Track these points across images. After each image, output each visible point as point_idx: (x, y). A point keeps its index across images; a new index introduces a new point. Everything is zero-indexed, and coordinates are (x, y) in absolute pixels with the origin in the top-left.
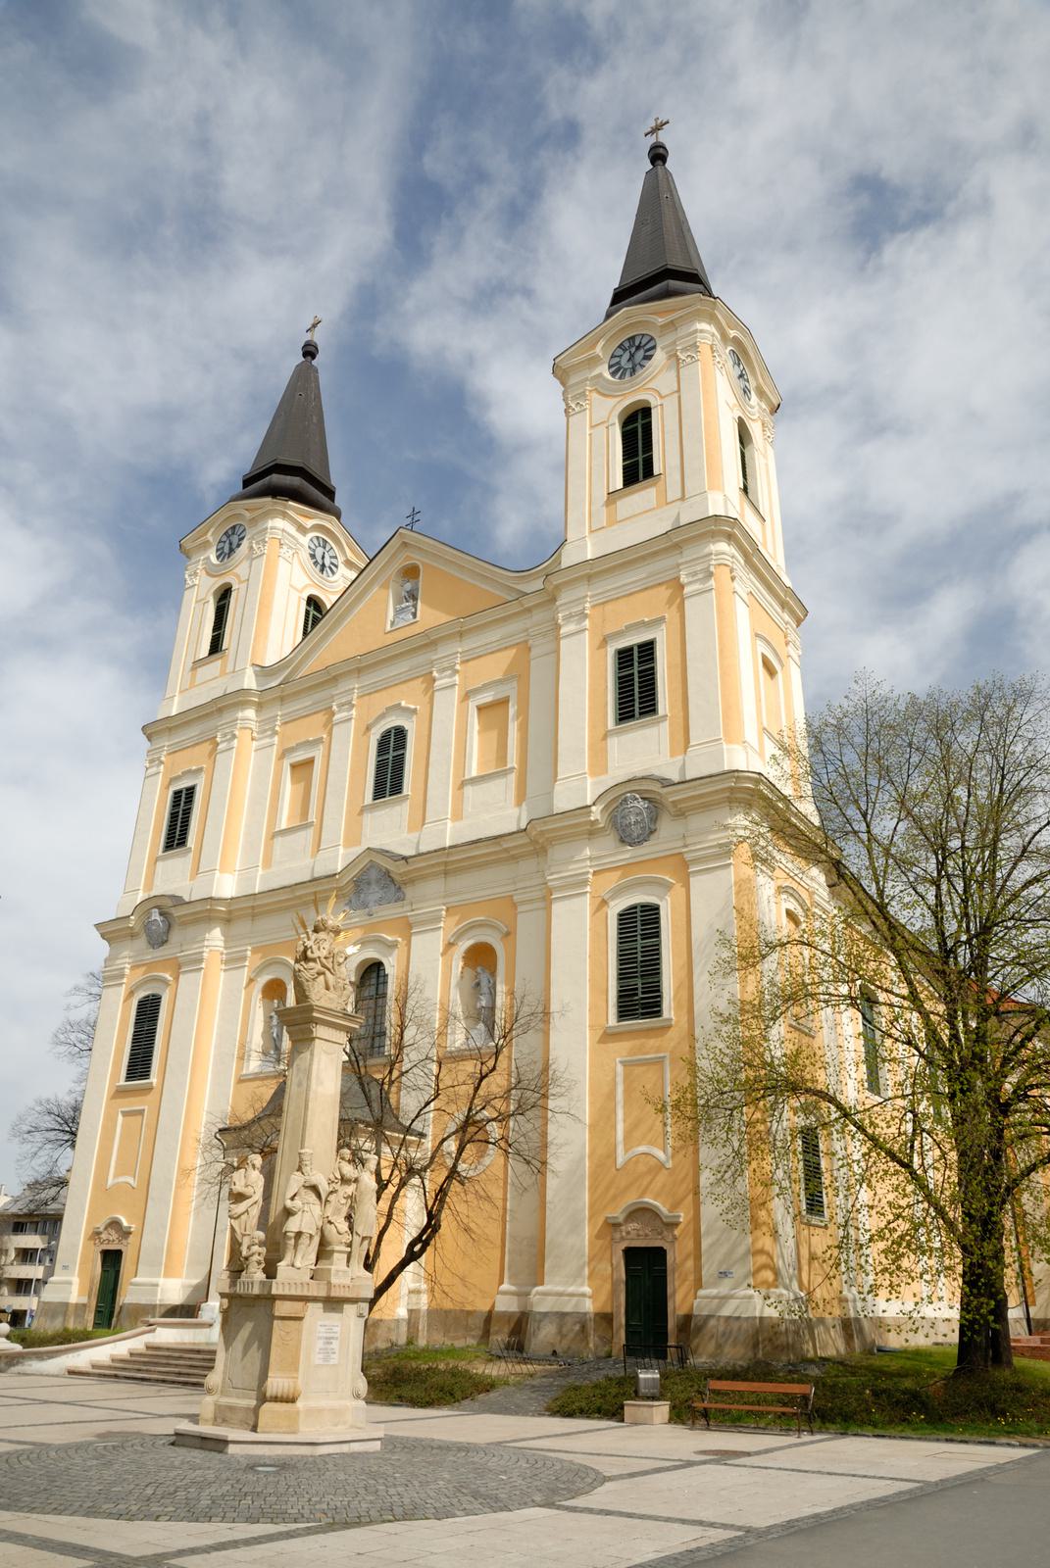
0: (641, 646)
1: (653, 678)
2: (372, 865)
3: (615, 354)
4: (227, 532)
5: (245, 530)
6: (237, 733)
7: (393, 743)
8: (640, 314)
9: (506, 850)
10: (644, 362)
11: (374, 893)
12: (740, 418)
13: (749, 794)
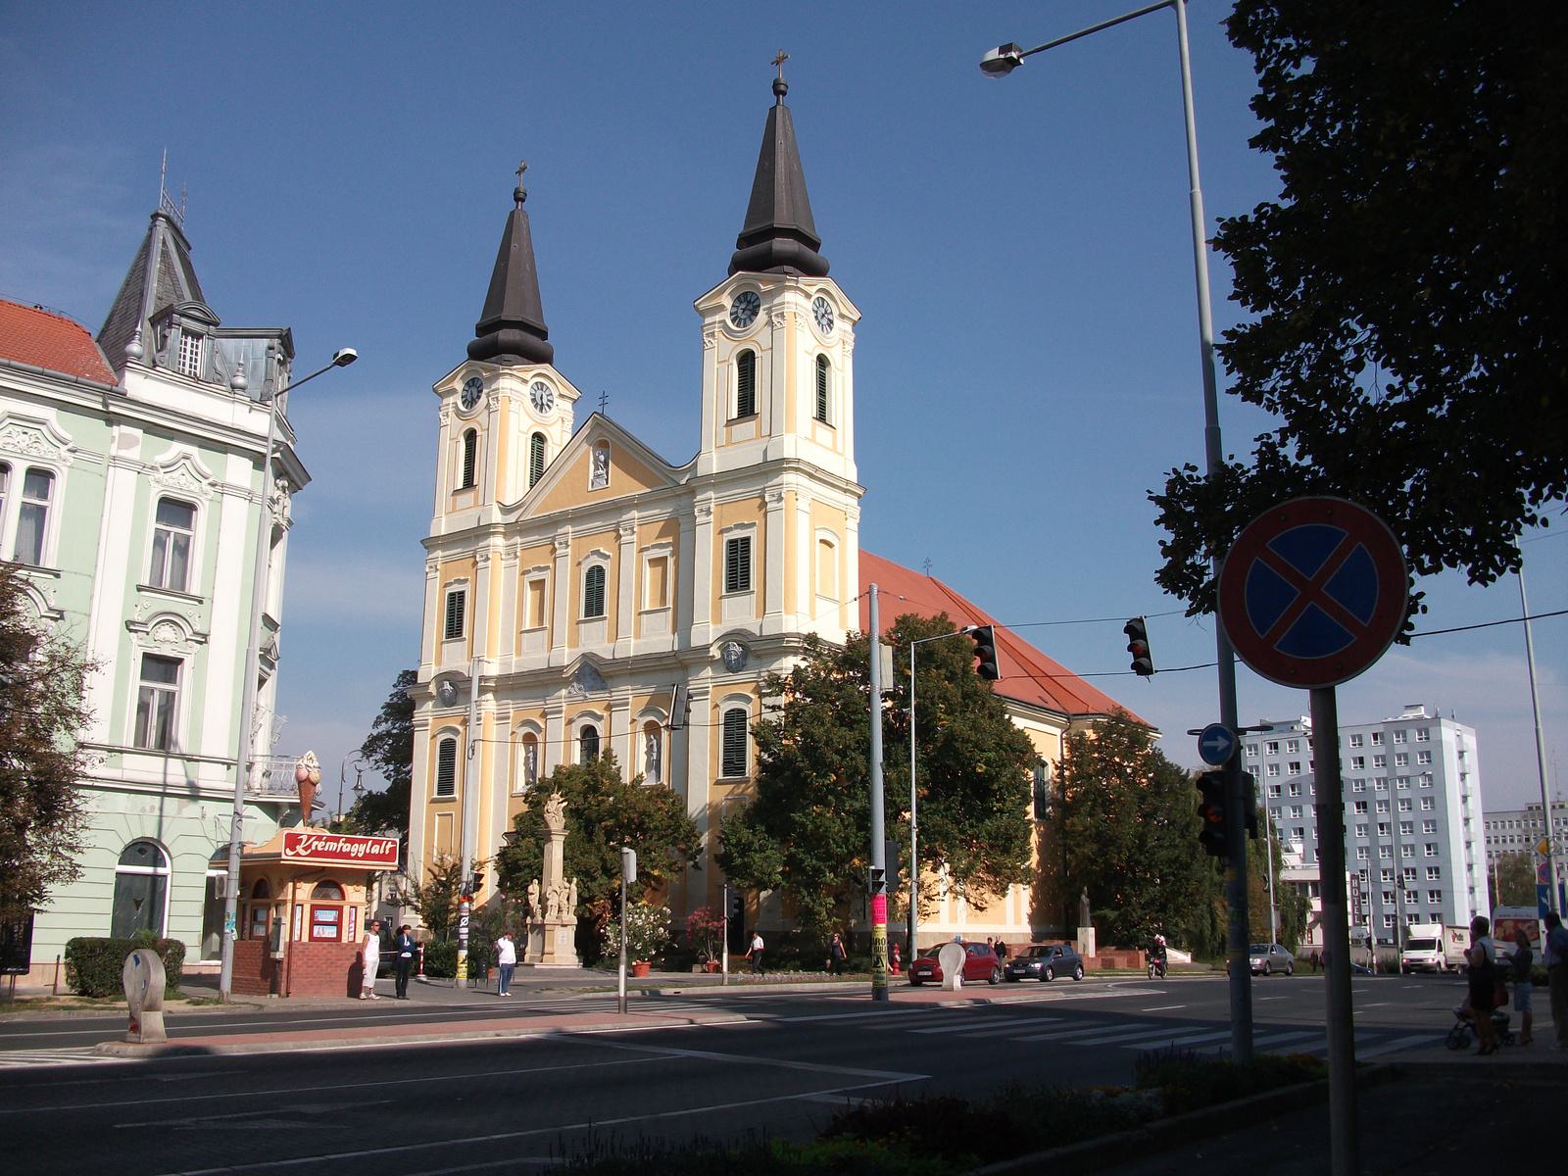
0: (742, 539)
6: (490, 556)
7: (596, 577)
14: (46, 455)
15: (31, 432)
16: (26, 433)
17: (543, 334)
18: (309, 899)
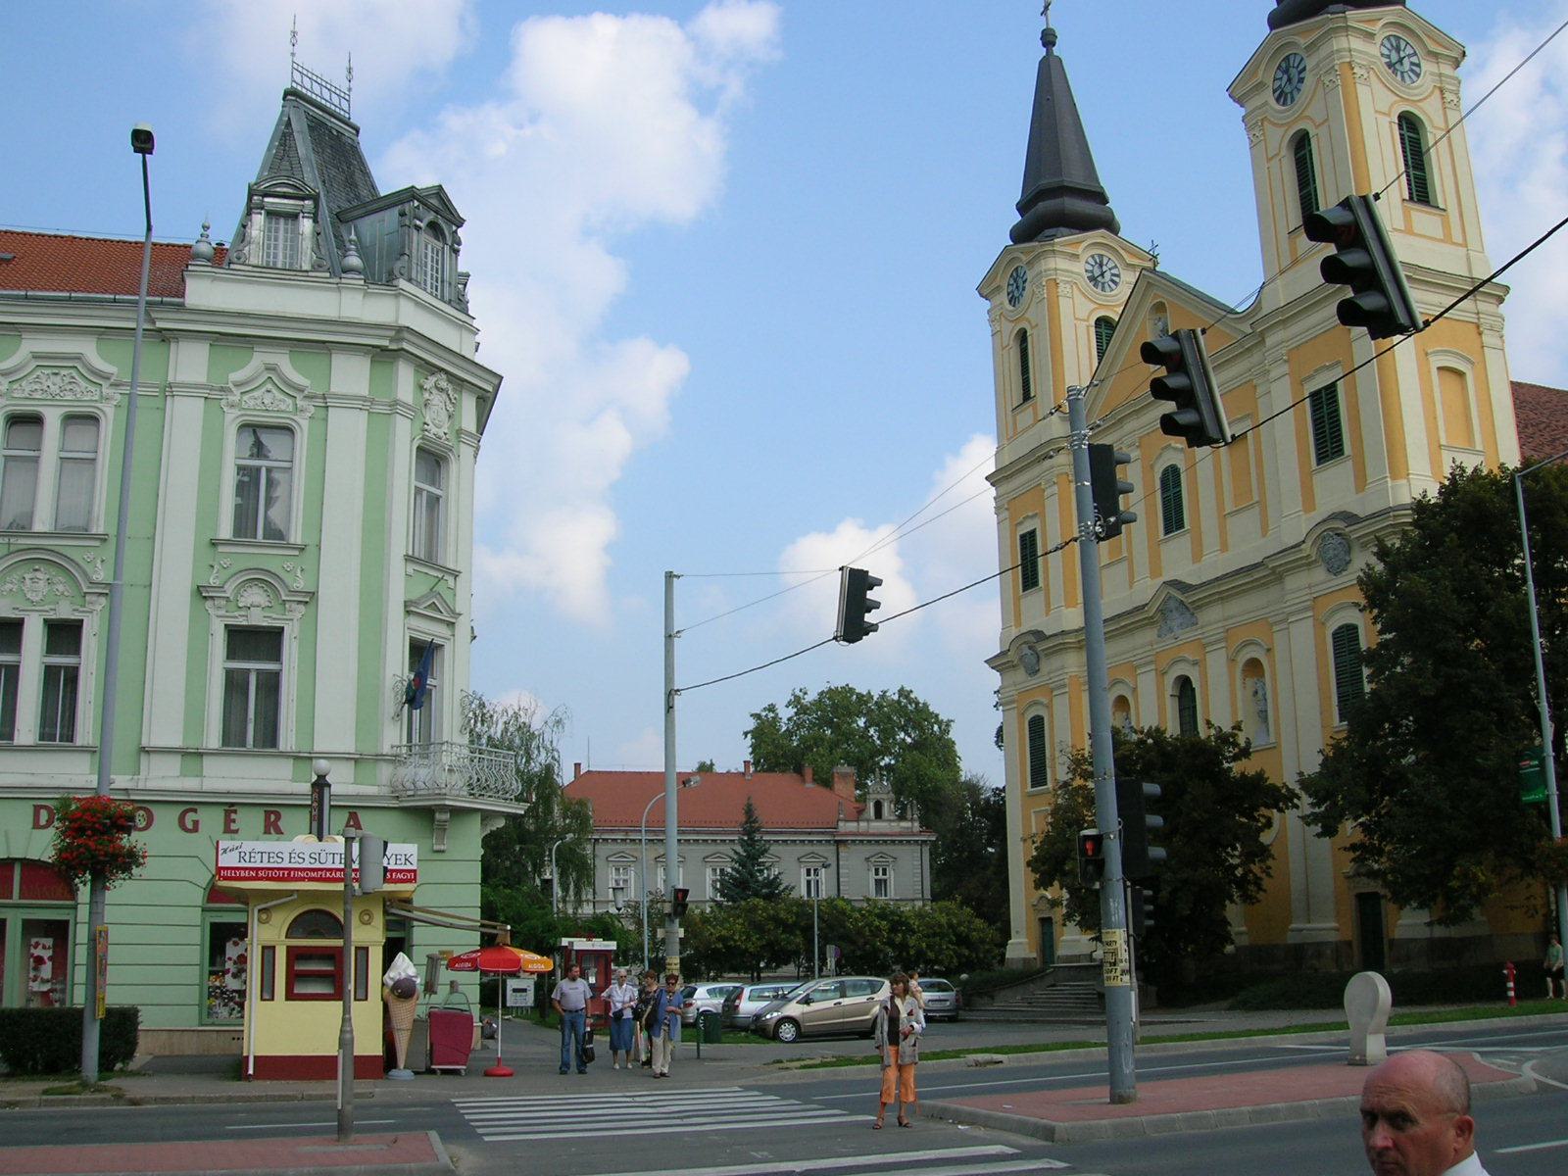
1: (1316, 430)
2: (1169, 597)
4: (1280, 65)
5: (1302, 59)
10: (1302, 75)
11: (1176, 620)
14: (85, 396)
15: (63, 372)
16: (56, 374)
17: (1100, 197)
18: (283, 937)
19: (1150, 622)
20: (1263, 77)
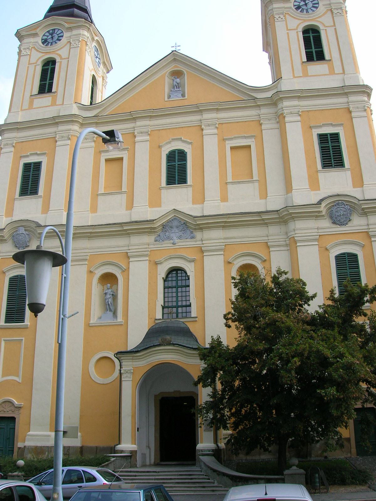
0: (35, 163)
3: (45, 34)
8: (63, 21)
9: (263, 220)
10: (57, 41)
12: (93, 75)
13: (10, 237)
19: (151, 231)
20: (39, 32)
